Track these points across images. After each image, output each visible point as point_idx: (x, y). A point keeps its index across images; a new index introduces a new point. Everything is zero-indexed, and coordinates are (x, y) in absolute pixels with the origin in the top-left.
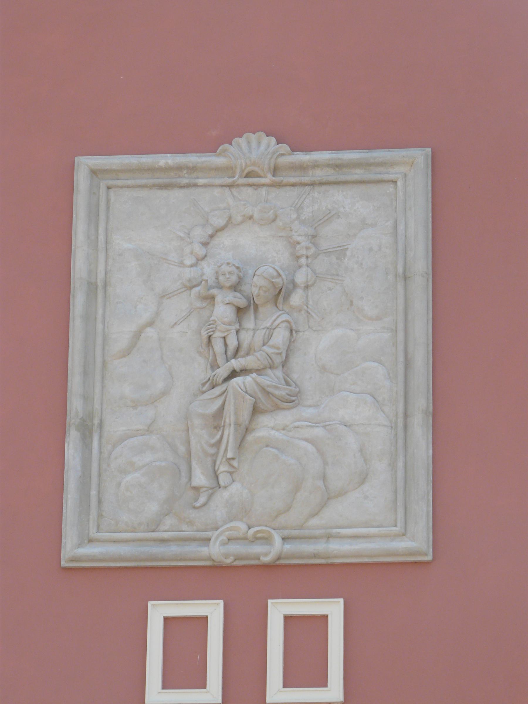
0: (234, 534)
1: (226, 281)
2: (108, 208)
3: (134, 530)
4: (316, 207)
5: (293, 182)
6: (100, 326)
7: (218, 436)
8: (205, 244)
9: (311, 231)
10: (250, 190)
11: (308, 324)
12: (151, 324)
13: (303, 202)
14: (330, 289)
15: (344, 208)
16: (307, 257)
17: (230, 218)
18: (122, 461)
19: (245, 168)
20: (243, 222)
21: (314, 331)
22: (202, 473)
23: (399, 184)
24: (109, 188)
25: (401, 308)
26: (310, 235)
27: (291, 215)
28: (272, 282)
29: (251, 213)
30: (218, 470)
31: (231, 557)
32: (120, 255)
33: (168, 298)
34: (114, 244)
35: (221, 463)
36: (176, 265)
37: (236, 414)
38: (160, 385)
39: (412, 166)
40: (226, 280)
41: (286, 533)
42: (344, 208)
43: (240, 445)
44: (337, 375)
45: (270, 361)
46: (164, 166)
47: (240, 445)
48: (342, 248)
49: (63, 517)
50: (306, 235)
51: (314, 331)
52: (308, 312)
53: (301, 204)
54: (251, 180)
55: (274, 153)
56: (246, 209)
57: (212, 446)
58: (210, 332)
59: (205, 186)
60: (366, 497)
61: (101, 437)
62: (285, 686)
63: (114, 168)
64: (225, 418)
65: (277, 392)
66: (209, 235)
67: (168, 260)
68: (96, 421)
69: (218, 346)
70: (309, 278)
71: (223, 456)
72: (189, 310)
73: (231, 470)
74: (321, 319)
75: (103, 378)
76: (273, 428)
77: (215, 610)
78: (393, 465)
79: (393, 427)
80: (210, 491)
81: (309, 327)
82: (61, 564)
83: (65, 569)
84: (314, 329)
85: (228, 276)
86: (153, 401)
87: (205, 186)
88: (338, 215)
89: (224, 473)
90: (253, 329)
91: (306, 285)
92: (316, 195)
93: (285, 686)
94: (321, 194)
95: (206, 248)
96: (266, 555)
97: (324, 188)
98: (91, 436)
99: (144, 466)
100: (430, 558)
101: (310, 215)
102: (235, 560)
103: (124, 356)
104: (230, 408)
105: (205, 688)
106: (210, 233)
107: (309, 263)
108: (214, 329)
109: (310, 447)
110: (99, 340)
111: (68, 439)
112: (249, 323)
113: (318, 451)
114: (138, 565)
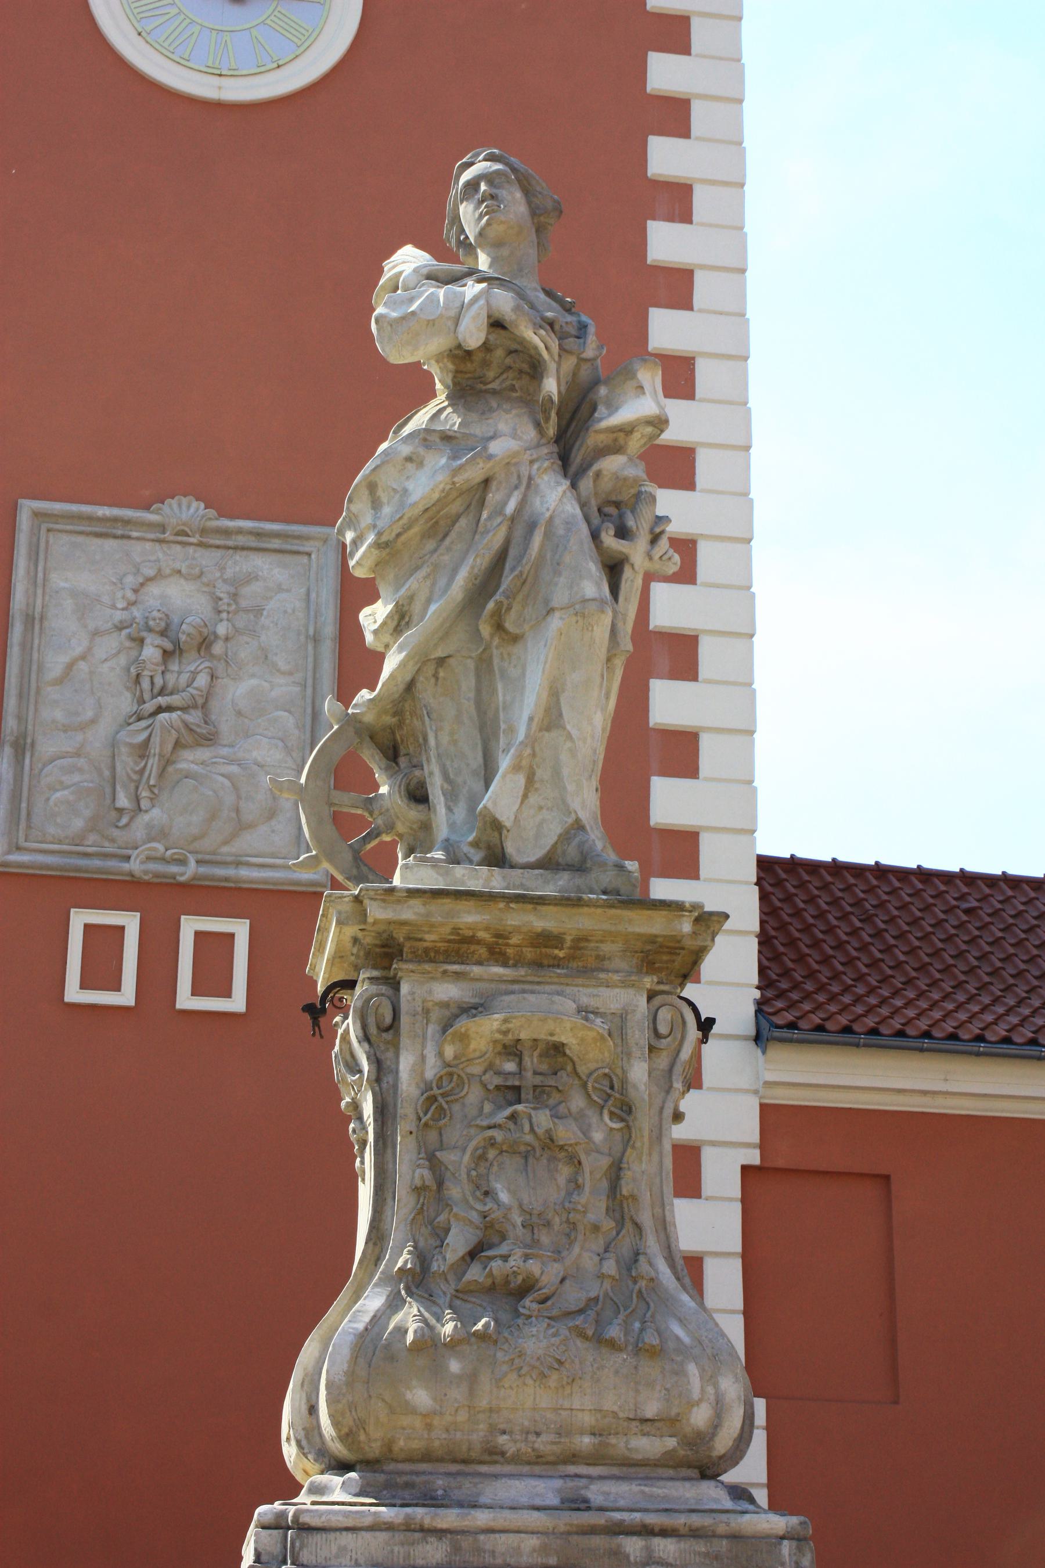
3: (60, 842)
4: (237, 569)
7: (142, 764)
8: (136, 591)
9: (232, 590)
10: (178, 548)
12: (83, 657)
16: (228, 612)
20: (170, 575)
23: (313, 556)
24: (49, 530)
25: (310, 667)
32: (57, 592)
37: (161, 746)
38: (90, 714)
41: (200, 857)
54: (180, 538)
59: (138, 539)
60: (273, 831)
61: (32, 756)
65: (198, 730)
73: (152, 796)
76: (192, 762)
81: (228, 675)
86: (82, 727)
87: (138, 539)
88: (256, 578)
92: (238, 558)
96: (182, 874)
97: (245, 553)
109: (227, 782)
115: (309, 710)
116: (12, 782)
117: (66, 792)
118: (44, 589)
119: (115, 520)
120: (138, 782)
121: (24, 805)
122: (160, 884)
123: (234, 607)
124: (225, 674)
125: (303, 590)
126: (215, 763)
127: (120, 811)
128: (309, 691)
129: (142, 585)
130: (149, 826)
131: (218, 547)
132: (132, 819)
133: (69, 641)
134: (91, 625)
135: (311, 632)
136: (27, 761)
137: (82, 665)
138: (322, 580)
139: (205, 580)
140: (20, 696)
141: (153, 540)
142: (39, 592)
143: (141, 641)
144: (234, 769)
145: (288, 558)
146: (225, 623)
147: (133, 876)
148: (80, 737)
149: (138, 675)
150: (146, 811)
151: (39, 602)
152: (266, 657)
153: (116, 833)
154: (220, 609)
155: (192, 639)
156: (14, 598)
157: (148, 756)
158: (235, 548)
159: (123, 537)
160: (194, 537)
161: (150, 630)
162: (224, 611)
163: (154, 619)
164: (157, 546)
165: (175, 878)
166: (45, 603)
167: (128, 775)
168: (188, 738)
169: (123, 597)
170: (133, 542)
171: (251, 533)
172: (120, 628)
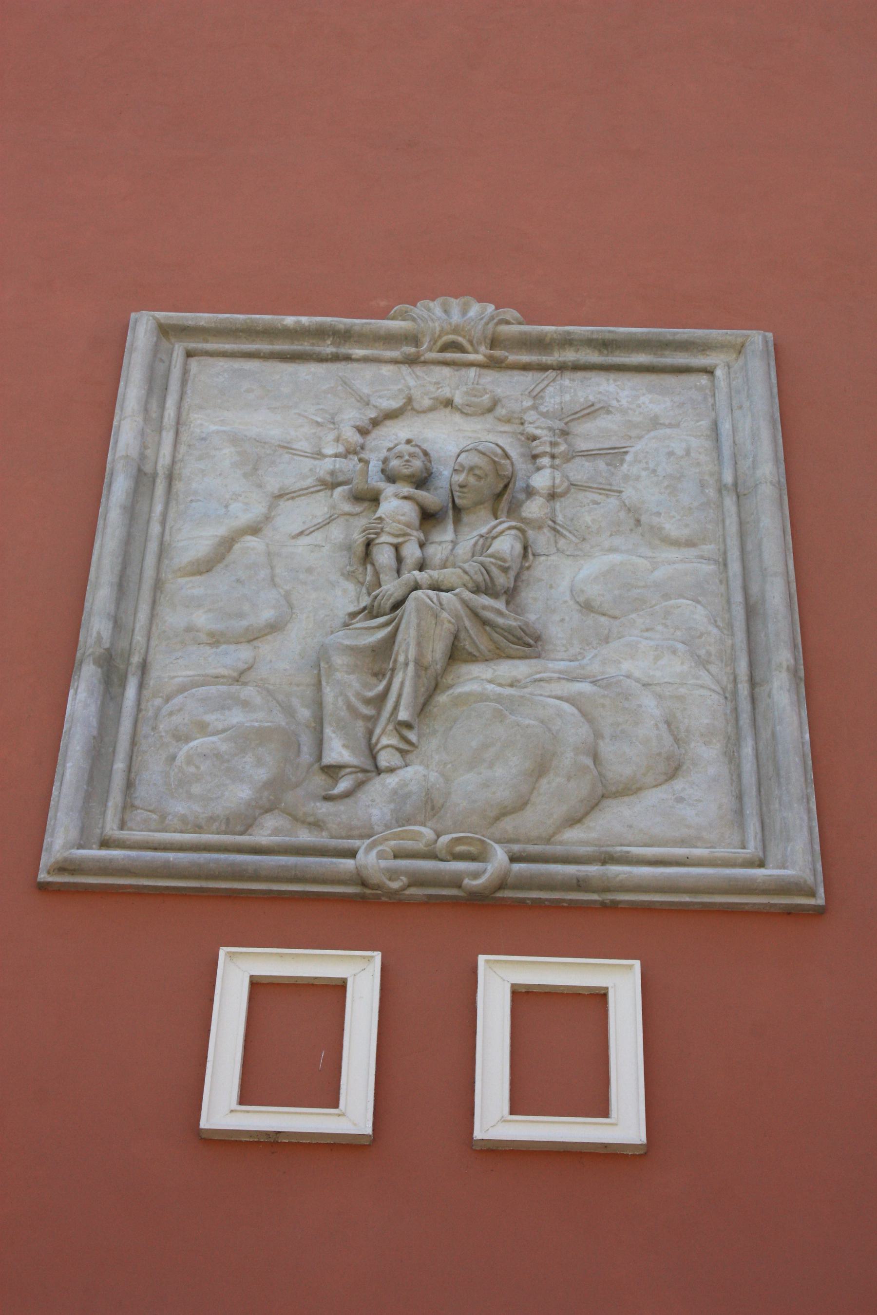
0: (409, 845)
1: (403, 466)
2: (184, 382)
3: (198, 828)
4: (567, 397)
5: (525, 361)
6: (155, 529)
7: (381, 687)
8: (363, 432)
9: (558, 425)
10: (446, 371)
11: (556, 546)
12: (254, 530)
13: (542, 390)
14: (597, 503)
15: (618, 401)
16: (553, 457)
17: (410, 400)
18: (184, 719)
19: (440, 337)
20: (432, 409)
21: (568, 556)
22: (344, 746)
23: (719, 373)
24: (189, 354)
25: (732, 528)
26: (558, 429)
27: (522, 402)
28: (494, 462)
29: (448, 395)
30: (377, 744)
31: (401, 878)
32: (204, 439)
33: (288, 499)
34: (192, 425)
35: (383, 732)
36: (307, 457)
37: (419, 644)
38: (267, 615)
39: (740, 352)
40: (404, 463)
41: (516, 848)
42: (618, 401)
43: (423, 707)
44: (615, 618)
45: (487, 576)
46: (292, 327)
47: (423, 707)
48: (616, 451)
49: (52, 803)
50: (550, 429)
51: (568, 556)
52: (555, 530)
53: (539, 393)
54: (449, 356)
55: (492, 318)
56: (440, 390)
57: (368, 702)
58: (370, 534)
59: (365, 360)
60: (680, 800)
61: (141, 686)
62: (512, 1112)
63: (201, 324)
64: (397, 655)
65: (500, 621)
66: (371, 419)
67: (292, 449)
68: (136, 659)
69: (386, 556)
70: (557, 481)
71: (389, 721)
72: (329, 516)
73: (403, 746)
74: (581, 539)
75: (154, 603)
76: (490, 682)
77: (363, 970)
78: (732, 757)
79: (729, 699)
80: (360, 776)
81: (558, 550)
82: (39, 877)
83: (44, 887)
84: (568, 553)
85: (407, 457)
86: (253, 637)
87: (365, 360)
88: (606, 409)
89: (389, 750)
90: (452, 542)
91: (551, 492)
92: (567, 382)
93: (512, 1112)
94: (575, 381)
95: (363, 438)
96: (476, 875)
97: (580, 375)
98: (123, 685)
99: (224, 731)
100: (820, 900)
101: (556, 407)
102: (409, 886)
103: (200, 573)
104: (408, 636)
105: (336, 1106)
106: (373, 416)
107: (556, 465)
108: (379, 531)
109: (566, 706)
110: (153, 547)
111: (76, 684)
112: (445, 535)
113: (584, 714)
114: (202, 886)
115: (738, 597)
116: (94, 722)
117: (214, 739)
118: (177, 433)
119: (320, 333)
120: (373, 720)
121: (119, 766)
122: (431, 902)
123: (563, 448)
124: (554, 550)
125: (705, 423)
126: (541, 680)
127: (333, 771)
128: (735, 567)
129: (375, 423)
130: (398, 796)
131: (525, 367)
132: (359, 785)
133: (226, 507)
134: (273, 485)
135: (728, 478)
136: (131, 692)
137: (251, 541)
138: (740, 407)
139: (501, 411)
140: (121, 587)
141: (395, 362)
142: (168, 437)
143: (373, 499)
144: (585, 687)
145: (671, 380)
146: (547, 472)
147: (364, 884)
148: (243, 654)
149: (368, 544)
150: (391, 770)
151: (166, 450)
152: (638, 522)
153: (324, 809)
154: (535, 452)
155: (479, 478)
156: (116, 442)
157: (393, 670)
158: (562, 368)
159: (336, 358)
160: (476, 352)
161: (392, 479)
162: (544, 454)
163: (399, 456)
164: (405, 369)
165: (459, 886)
166: (179, 456)
167: (350, 707)
168: (481, 641)
169: (337, 440)
170: (356, 365)
171: (591, 343)
172: (330, 484)
